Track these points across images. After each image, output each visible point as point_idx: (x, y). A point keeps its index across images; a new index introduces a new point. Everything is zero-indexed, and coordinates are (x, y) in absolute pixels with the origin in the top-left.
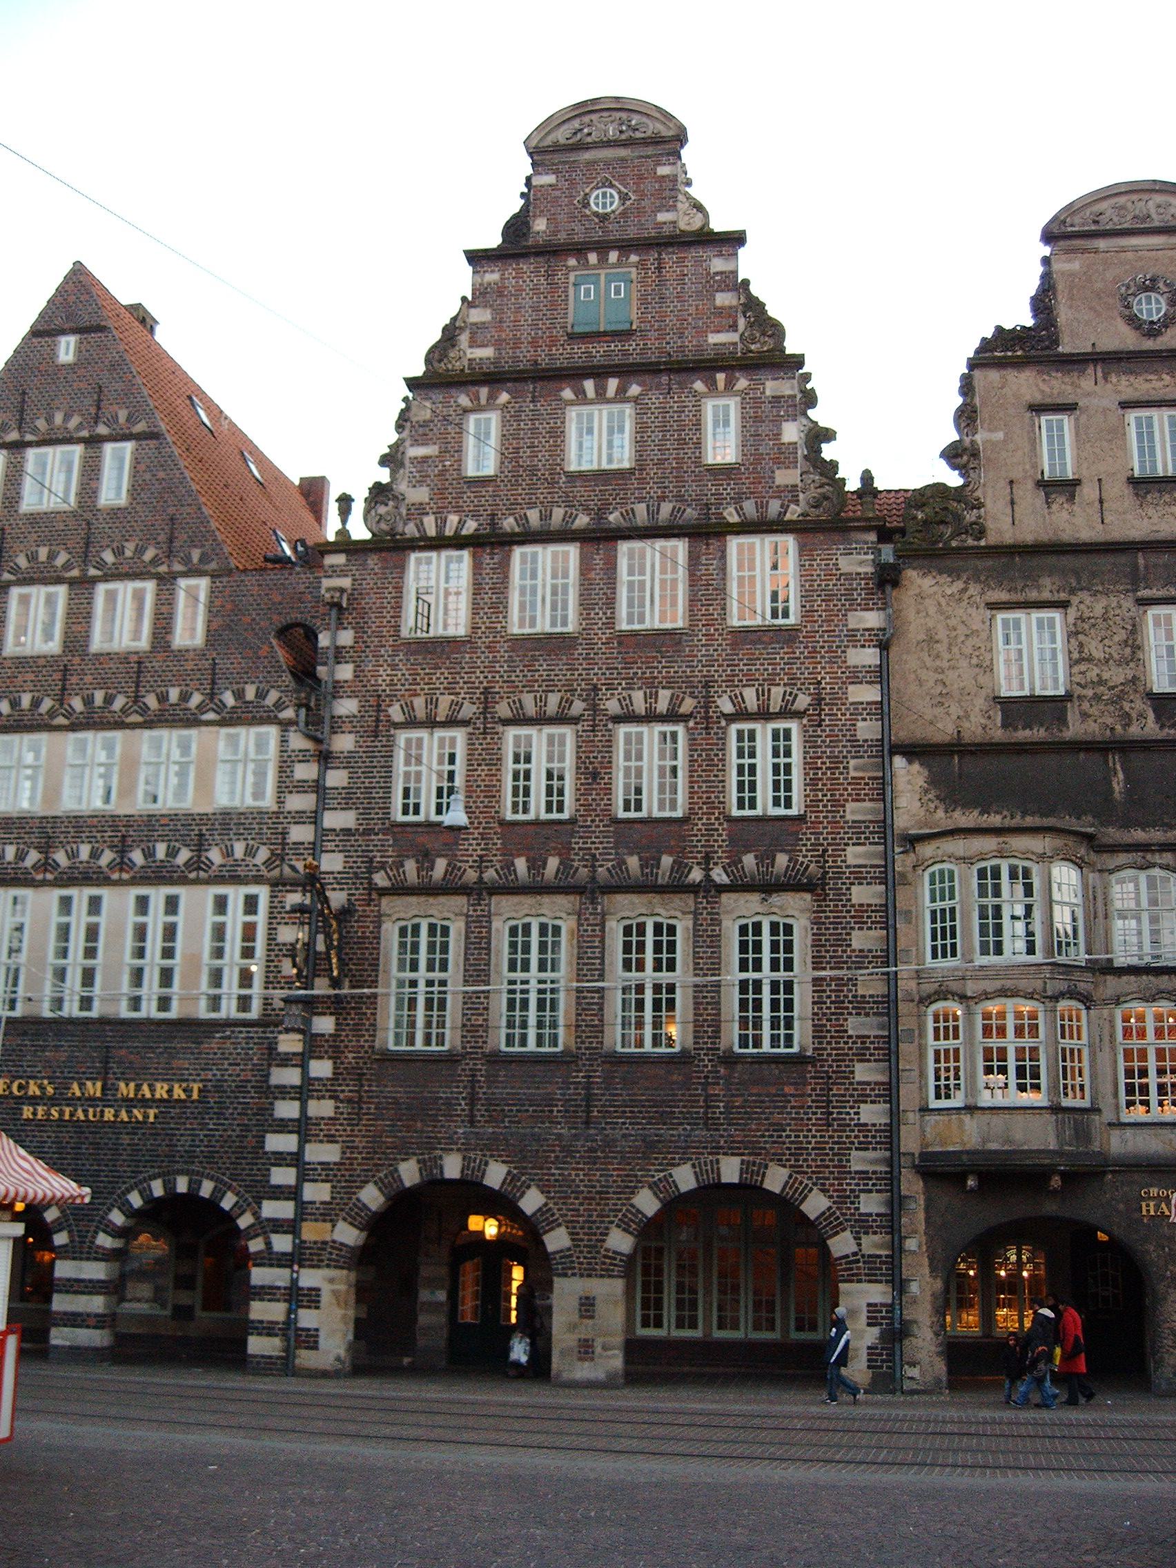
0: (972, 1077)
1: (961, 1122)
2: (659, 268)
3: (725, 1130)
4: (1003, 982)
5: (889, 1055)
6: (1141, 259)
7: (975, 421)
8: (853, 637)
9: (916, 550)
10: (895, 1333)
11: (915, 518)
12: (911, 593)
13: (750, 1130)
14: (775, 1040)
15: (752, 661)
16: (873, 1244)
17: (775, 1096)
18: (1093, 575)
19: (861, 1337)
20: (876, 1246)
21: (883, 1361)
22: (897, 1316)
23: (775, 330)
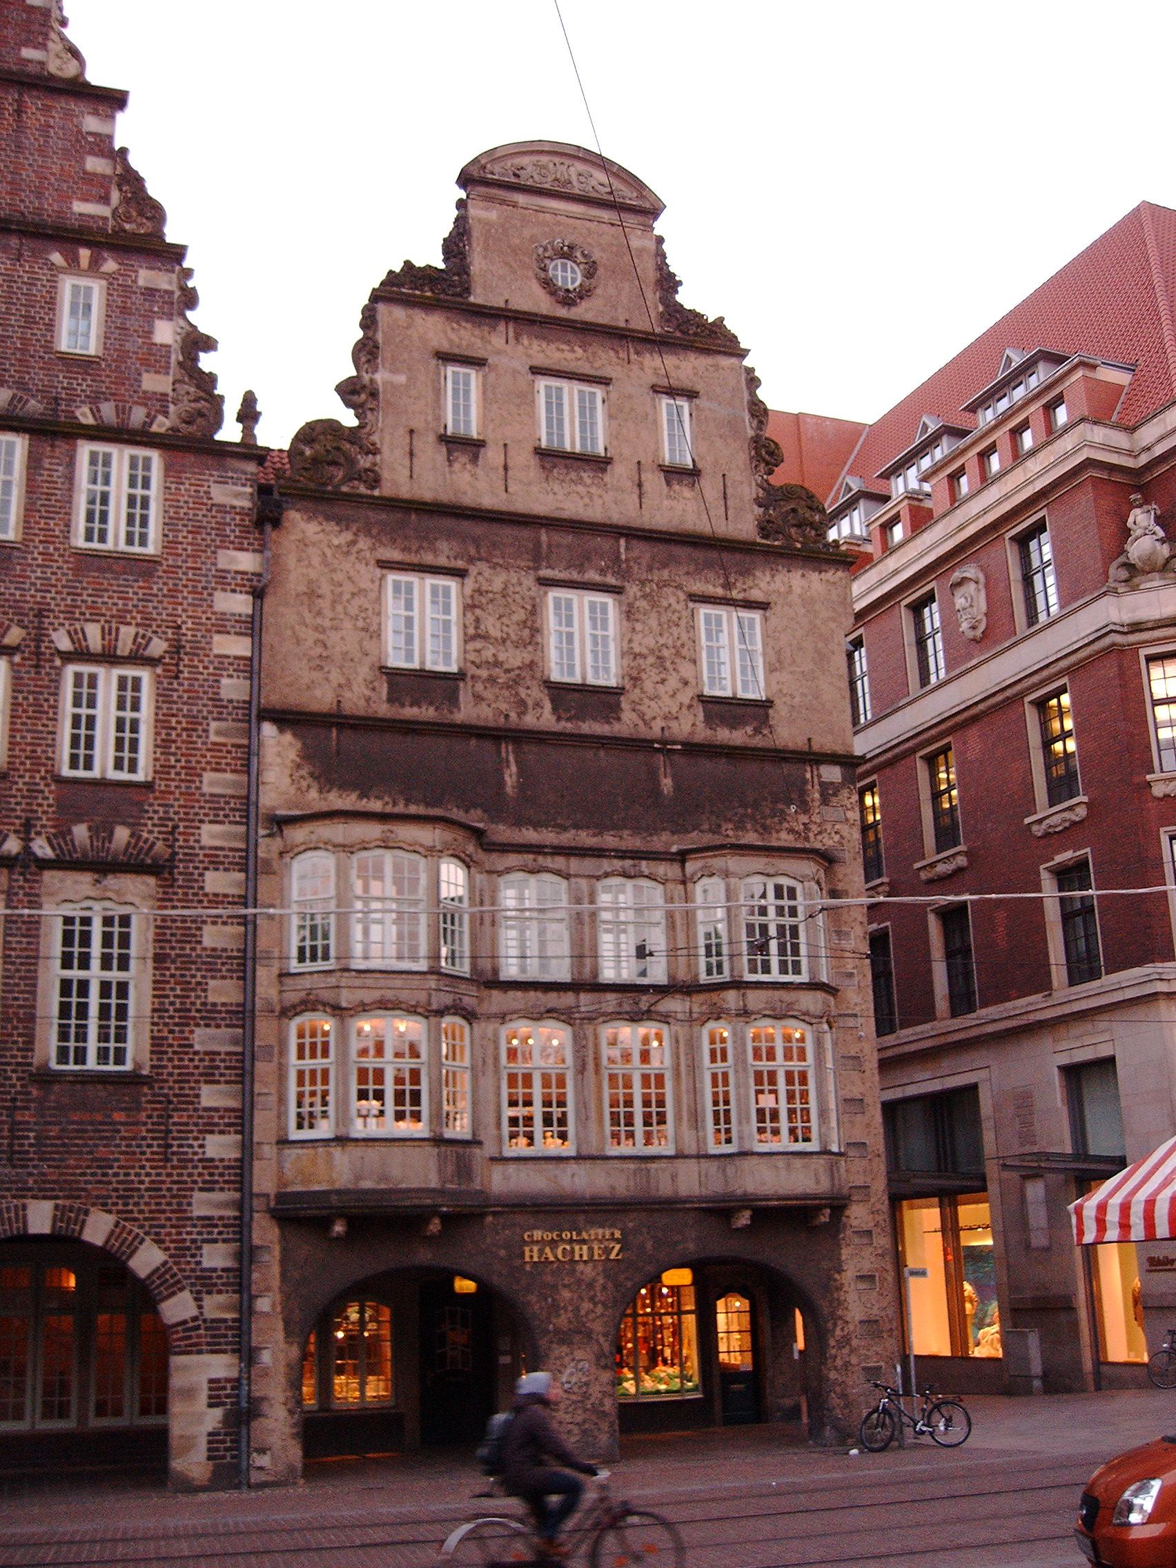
0: (343, 1104)
1: (329, 1154)
2: (19, 112)
3: (35, 1167)
4: (383, 992)
5: (242, 1075)
6: (559, 223)
7: (376, 358)
8: (223, 580)
9: (302, 489)
10: (241, 1412)
11: (302, 453)
12: (293, 538)
13: (67, 1167)
14: (103, 1055)
15: (98, 592)
16: (217, 1306)
17: (101, 1123)
18: (494, 545)
19: (194, 1422)
20: (222, 1308)
21: (226, 1449)
22: (244, 1393)
23: (155, 212)
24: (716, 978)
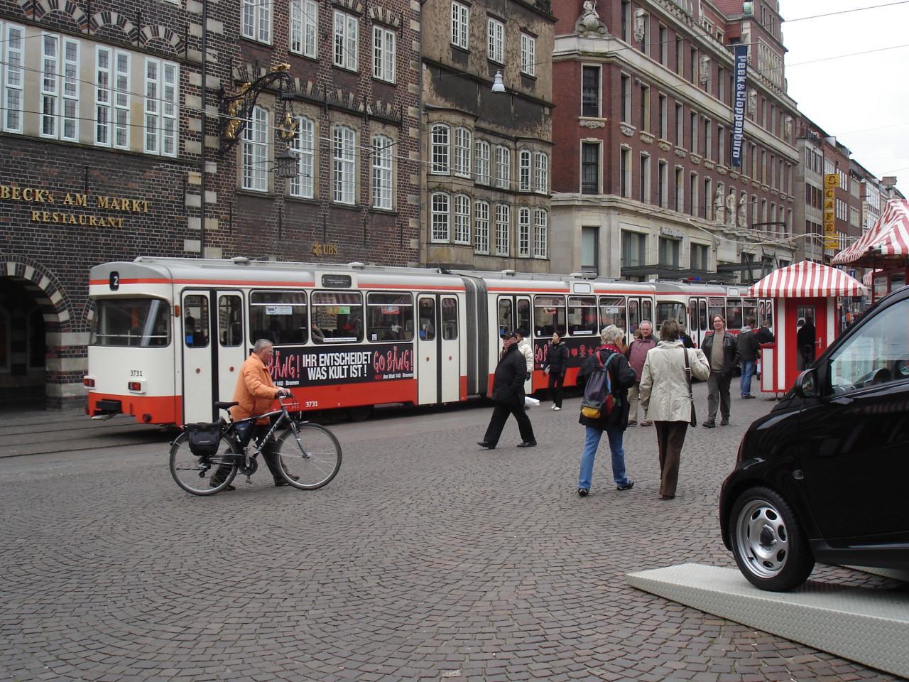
24: (525, 190)
